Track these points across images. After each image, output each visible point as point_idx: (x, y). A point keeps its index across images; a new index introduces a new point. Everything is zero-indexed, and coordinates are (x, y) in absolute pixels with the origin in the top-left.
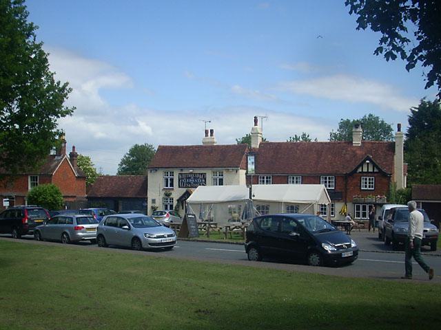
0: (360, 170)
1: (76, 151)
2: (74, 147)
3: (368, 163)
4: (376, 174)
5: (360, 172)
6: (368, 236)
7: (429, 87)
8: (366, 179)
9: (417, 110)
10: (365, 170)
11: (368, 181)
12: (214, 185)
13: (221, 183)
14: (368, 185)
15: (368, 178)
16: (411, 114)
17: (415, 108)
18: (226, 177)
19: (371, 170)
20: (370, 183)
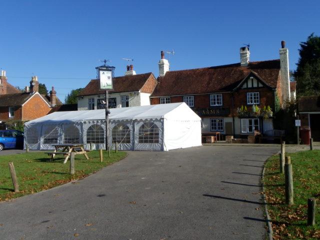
0: (245, 86)
1: (55, 90)
2: (53, 88)
3: (252, 80)
4: (260, 90)
5: (245, 89)
6: (39, 157)
7: (146, 74)
8: (251, 95)
9: (306, 45)
10: (250, 86)
11: (253, 97)
12: (90, 109)
13: (127, 106)
14: (216, 101)
15: (253, 93)
16: (300, 48)
17: (305, 43)
18: (131, 102)
19: (255, 85)
20: (255, 98)
